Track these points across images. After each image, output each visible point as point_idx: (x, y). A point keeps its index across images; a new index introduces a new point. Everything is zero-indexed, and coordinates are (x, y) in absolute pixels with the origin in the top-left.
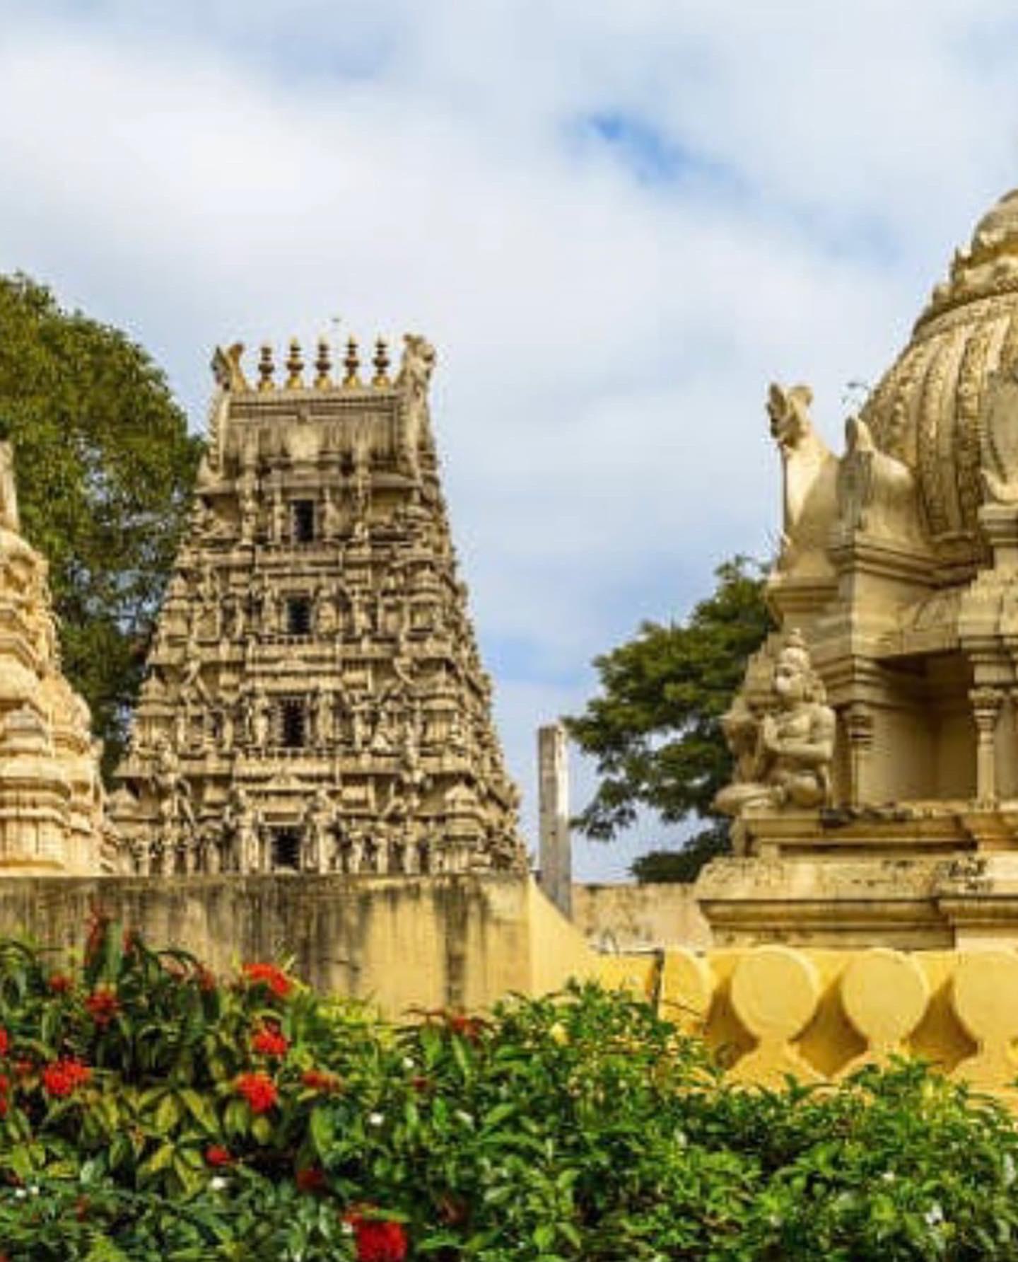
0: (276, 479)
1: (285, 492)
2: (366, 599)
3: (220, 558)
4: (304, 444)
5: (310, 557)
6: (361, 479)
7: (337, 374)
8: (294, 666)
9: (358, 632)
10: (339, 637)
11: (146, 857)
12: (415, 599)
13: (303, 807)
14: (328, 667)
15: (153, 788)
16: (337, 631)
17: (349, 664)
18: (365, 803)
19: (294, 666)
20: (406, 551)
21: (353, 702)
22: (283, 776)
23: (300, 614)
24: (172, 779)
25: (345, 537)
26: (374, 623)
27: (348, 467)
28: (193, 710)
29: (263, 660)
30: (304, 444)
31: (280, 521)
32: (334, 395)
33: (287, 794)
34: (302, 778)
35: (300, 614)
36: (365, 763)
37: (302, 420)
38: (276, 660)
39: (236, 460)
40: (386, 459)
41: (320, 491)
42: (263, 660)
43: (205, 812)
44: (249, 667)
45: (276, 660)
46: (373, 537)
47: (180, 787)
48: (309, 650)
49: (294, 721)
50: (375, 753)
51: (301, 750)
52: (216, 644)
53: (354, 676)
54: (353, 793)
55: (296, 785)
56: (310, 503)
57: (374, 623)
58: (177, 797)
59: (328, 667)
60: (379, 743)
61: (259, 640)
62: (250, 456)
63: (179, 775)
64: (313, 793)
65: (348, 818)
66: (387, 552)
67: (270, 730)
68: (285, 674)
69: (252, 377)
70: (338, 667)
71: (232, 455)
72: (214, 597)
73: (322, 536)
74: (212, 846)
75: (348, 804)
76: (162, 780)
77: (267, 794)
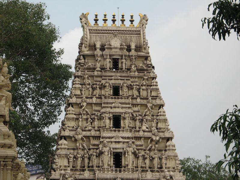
0: (107, 52)
1: (110, 56)
2: (138, 87)
3: (91, 73)
4: (116, 43)
5: (119, 74)
6: (133, 53)
7: (118, 23)
8: (118, 107)
9: (135, 96)
10: (130, 97)
11: (71, 160)
12: (152, 87)
13: (125, 146)
14: (128, 106)
15: (73, 139)
16: (129, 96)
17: (134, 105)
18: (141, 146)
19: (118, 107)
20: (148, 74)
21: (137, 116)
22: (118, 137)
23: (116, 91)
24: (80, 137)
25: (129, 69)
26: (139, 94)
27: (129, 50)
28: (85, 117)
29: (107, 103)
30: (116, 43)
31: (108, 64)
32: (118, 29)
33: (119, 142)
34: (123, 138)
35: (116, 91)
36: (141, 134)
37: (115, 36)
38: (112, 103)
39: (95, 45)
40: (139, 48)
41: (122, 56)
42: (107, 103)
43: (91, 147)
44: (103, 105)
45: (112, 103)
46: (137, 70)
47: (82, 139)
48: (120, 100)
49: (117, 121)
50: (144, 131)
51: (121, 129)
52: (92, 98)
53: (136, 109)
54: (138, 143)
55: (121, 140)
56: (118, 59)
57: (139, 94)
58: (81, 141)
59: (128, 106)
60: (144, 128)
61: (105, 98)
62: (98, 46)
63: (82, 136)
64: (128, 142)
65: (138, 150)
66: (143, 74)
67: (110, 124)
68: (115, 107)
69: (92, 22)
70: (130, 106)
71: (92, 44)
72: (89, 84)
73: (122, 69)
74: (95, 157)
75: (137, 146)
76: (76, 137)
77: (112, 142)
